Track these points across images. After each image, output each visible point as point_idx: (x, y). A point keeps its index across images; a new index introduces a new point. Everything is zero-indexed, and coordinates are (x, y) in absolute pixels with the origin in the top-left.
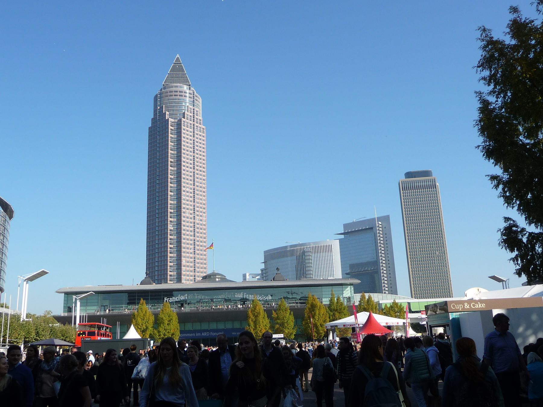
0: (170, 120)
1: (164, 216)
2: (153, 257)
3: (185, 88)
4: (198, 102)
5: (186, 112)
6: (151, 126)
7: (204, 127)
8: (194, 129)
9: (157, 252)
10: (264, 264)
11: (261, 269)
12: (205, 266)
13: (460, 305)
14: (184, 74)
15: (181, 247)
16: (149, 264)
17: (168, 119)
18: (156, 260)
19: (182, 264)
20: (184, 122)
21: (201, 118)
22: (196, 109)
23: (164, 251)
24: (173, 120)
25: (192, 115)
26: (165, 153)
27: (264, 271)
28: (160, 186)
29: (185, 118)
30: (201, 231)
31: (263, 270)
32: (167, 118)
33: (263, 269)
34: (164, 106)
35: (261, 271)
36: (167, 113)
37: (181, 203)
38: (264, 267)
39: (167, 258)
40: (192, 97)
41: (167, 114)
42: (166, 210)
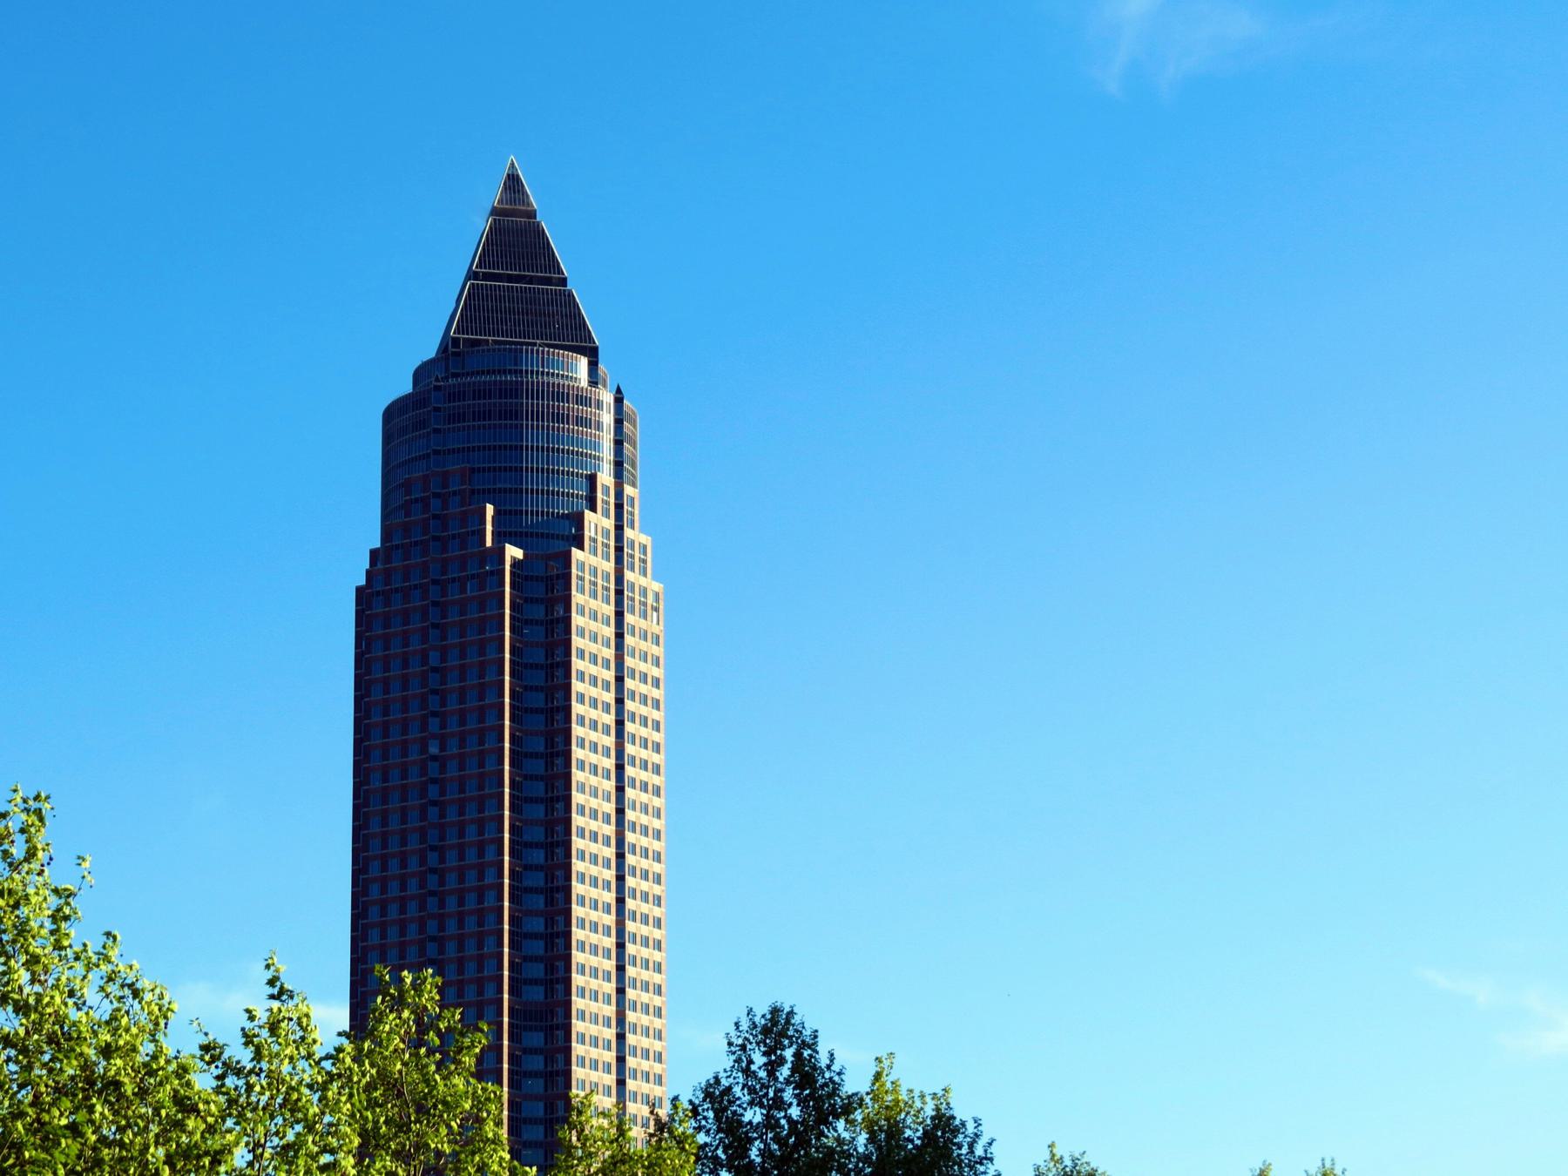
7: (656, 586)
20: (582, 566)
21: (644, 539)
32: (489, 543)
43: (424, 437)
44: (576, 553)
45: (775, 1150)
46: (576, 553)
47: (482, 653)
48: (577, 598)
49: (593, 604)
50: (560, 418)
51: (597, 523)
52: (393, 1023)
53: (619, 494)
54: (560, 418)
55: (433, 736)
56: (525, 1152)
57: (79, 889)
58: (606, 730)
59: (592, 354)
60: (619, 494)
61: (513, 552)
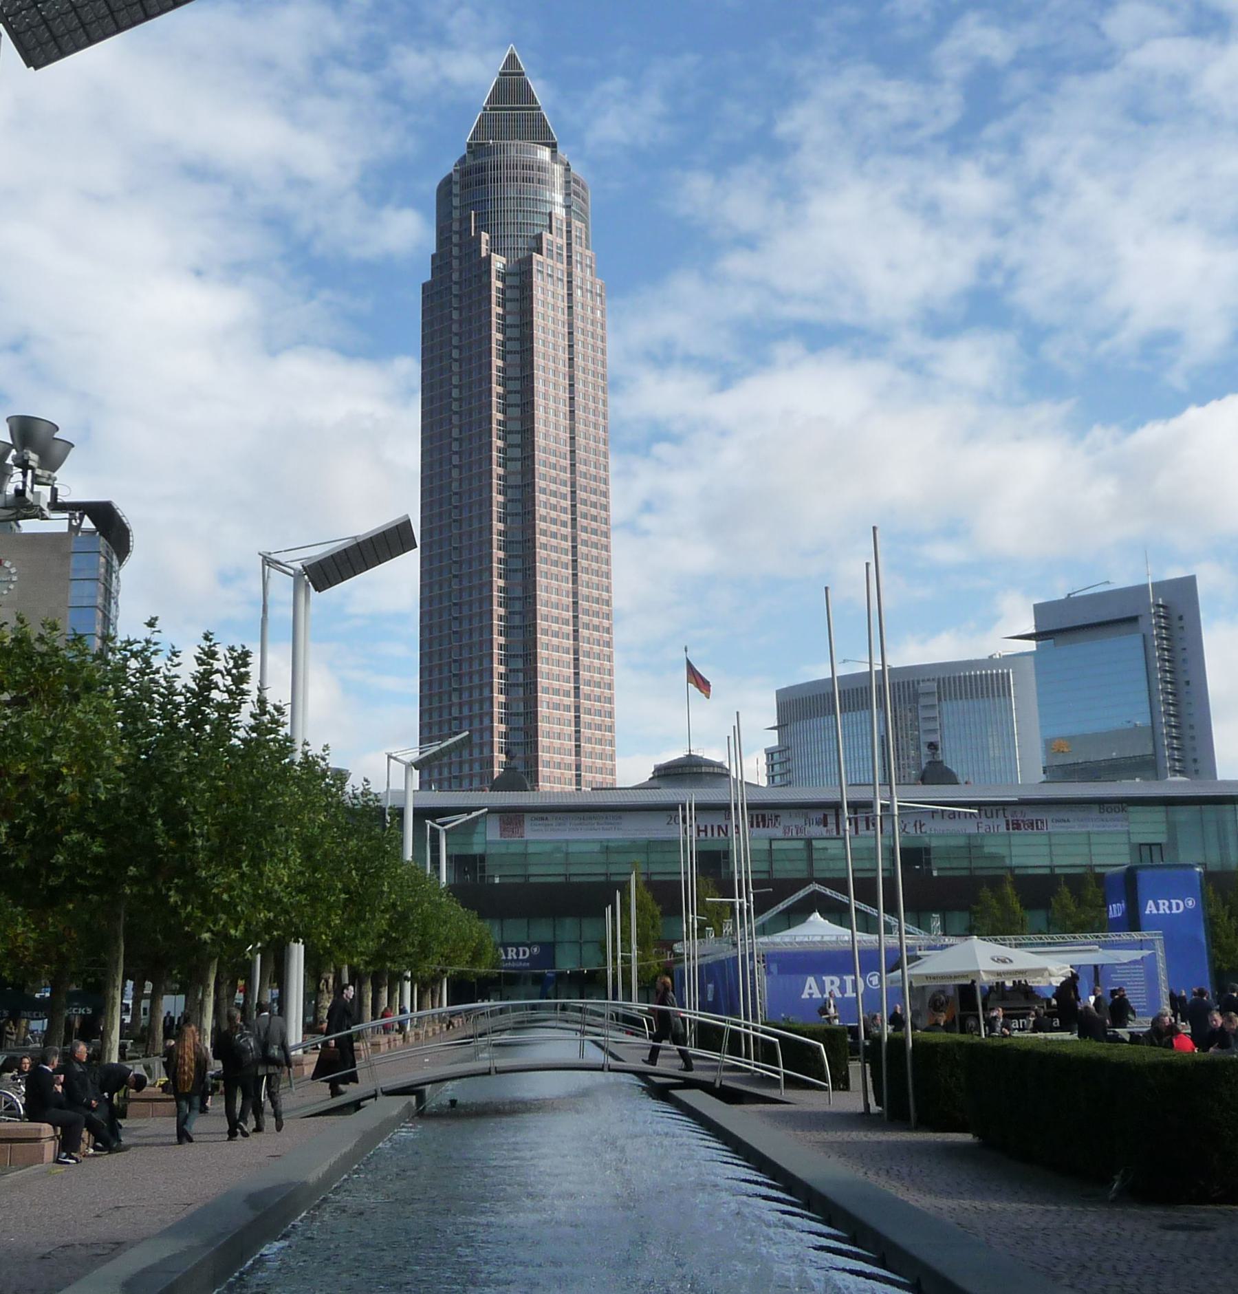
2: (444, 522)
3: (544, 154)
4: (580, 200)
5: (546, 236)
6: (429, 278)
9: (458, 559)
10: (776, 731)
11: (766, 750)
12: (606, 623)
13: (1174, 902)
14: (533, 109)
15: (536, 642)
16: (430, 683)
17: (489, 257)
18: (455, 380)
19: (540, 774)
22: (576, 223)
23: (481, 687)
25: (562, 241)
26: (480, 393)
27: (776, 756)
28: (464, 475)
29: (542, 254)
30: (594, 525)
31: (772, 754)
32: (484, 254)
33: (772, 748)
34: (473, 212)
35: (768, 754)
36: (485, 236)
37: (534, 501)
38: (777, 744)
39: (492, 649)
40: (569, 521)
41: (483, 241)
42: (484, 566)
44: (536, 257)
46: (536, 257)
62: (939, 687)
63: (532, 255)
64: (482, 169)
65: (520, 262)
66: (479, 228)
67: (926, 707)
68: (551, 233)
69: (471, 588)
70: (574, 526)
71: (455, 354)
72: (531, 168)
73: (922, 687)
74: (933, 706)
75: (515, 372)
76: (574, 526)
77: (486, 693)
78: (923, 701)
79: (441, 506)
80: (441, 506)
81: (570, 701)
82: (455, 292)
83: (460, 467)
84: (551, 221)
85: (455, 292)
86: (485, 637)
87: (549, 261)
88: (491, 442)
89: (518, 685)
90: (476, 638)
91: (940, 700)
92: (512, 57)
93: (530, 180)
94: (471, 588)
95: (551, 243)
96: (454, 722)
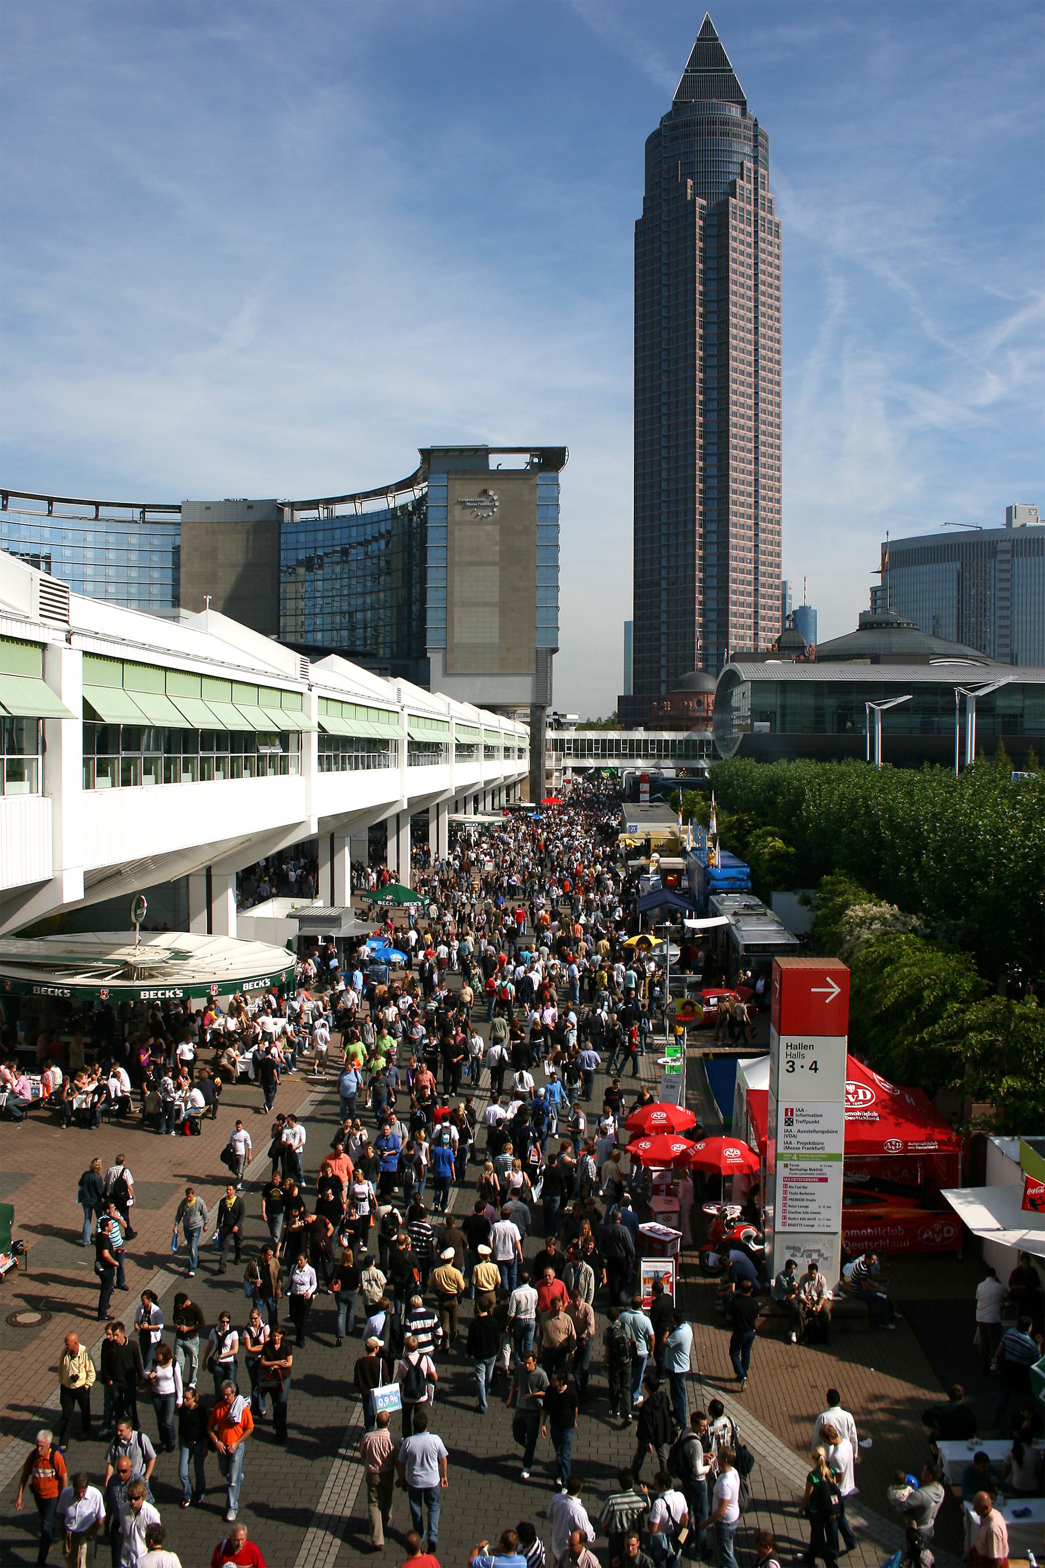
0: (700, 201)
1: (685, 523)
5: (739, 182)
8: (756, 226)
24: (704, 202)
25: (751, 187)
32: (689, 198)
36: (690, 182)
41: (689, 187)
43: (721, 1026)
44: (732, 200)
45: (911, 1495)
46: (732, 200)
47: (686, 504)
48: (732, 222)
49: (742, 226)
50: (726, 134)
51: (745, 186)
52: (360, 616)
53: (756, 172)
54: (726, 134)
55: (664, 682)
56: (997, 1142)
57: (309, 564)
58: (749, 235)
59: (743, 104)
60: (756, 172)
61: (700, 201)
62: (1013, 546)
63: (728, 200)
64: (688, 124)
65: (718, 204)
66: (685, 176)
67: (1001, 561)
68: (742, 179)
69: (677, 567)
70: (756, 420)
71: (664, 452)
72: (727, 123)
73: (1000, 546)
74: (1008, 561)
75: (712, 605)
76: (756, 420)
77: (690, 527)
78: (1000, 557)
79: (652, 521)
80: (652, 521)
81: (751, 555)
82: (664, 314)
83: (668, 415)
84: (742, 170)
85: (664, 314)
86: (689, 573)
87: (741, 204)
88: (695, 530)
89: (713, 356)
90: (681, 507)
91: (1013, 556)
92: (707, 24)
93: (727, 134)
94: (677, 567)
95: (742, 188)
96: (663, 364)
